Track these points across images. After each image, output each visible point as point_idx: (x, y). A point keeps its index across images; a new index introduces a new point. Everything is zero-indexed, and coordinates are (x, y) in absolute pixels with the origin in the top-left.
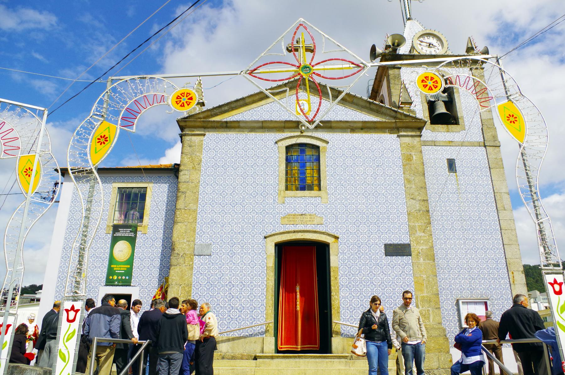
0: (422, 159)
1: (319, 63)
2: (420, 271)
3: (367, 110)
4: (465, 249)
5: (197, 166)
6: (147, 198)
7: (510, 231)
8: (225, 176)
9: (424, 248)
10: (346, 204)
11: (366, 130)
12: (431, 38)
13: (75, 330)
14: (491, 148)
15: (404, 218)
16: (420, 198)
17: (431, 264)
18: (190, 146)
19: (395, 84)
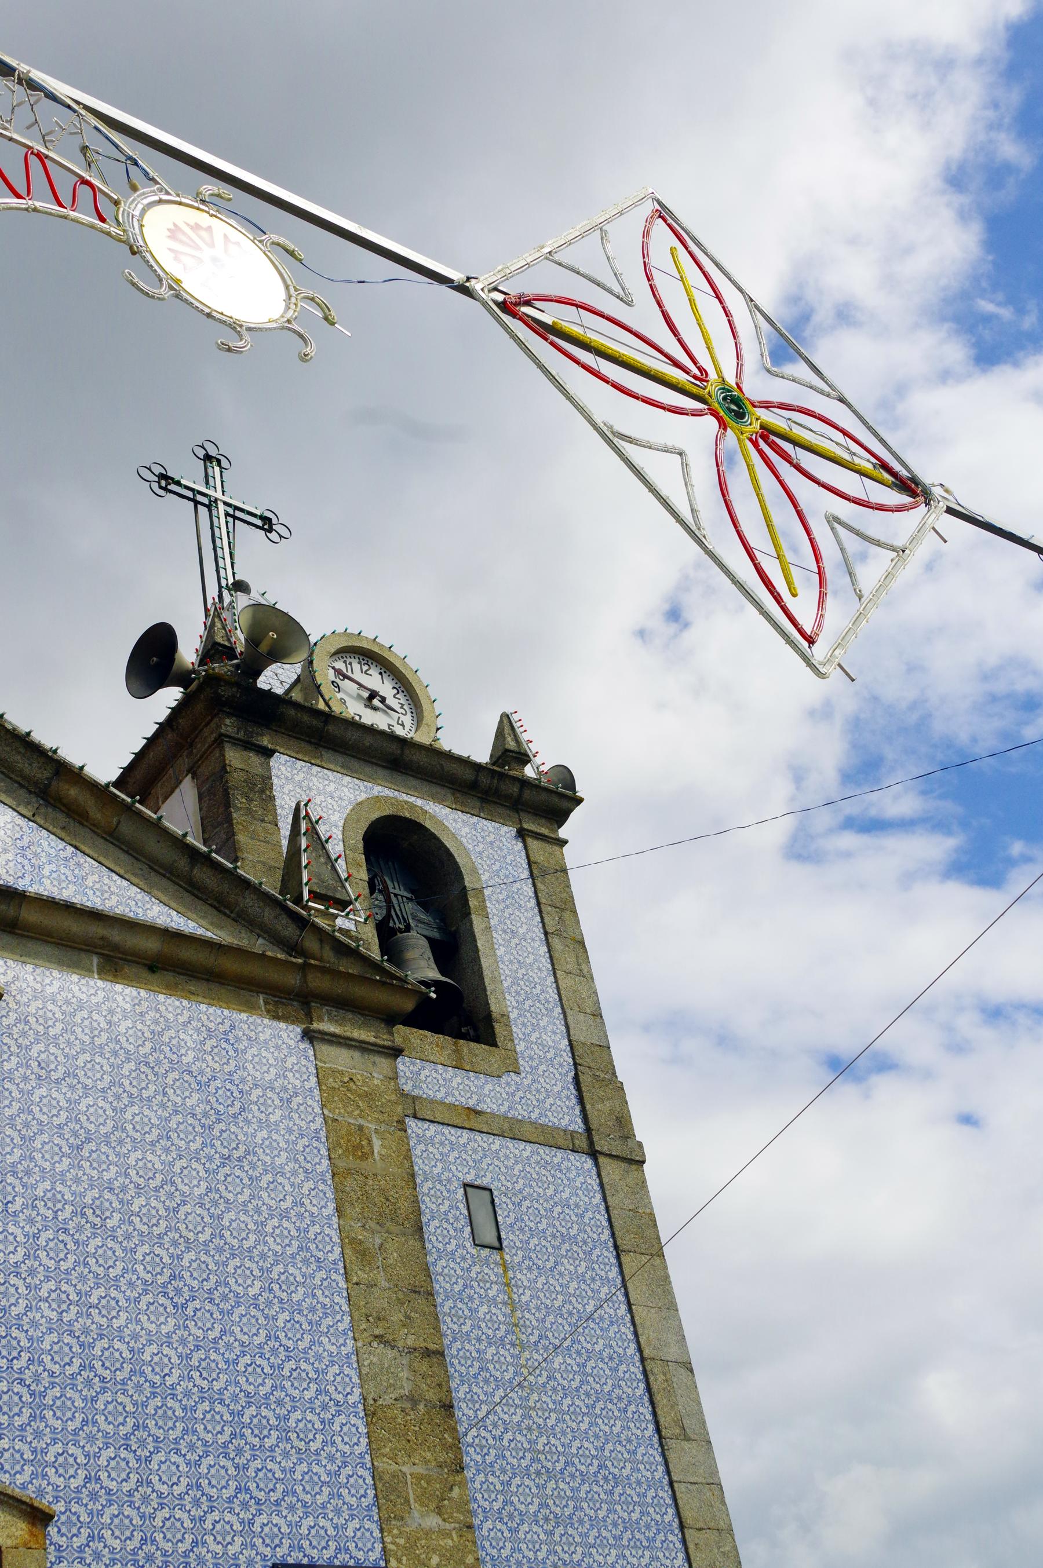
0: (408, 1157)
3: (172, 887)
7: (713, 1536)
10: (86, 1331)
11: (169, 976)
12: (374, 672)
15: (352, 1433)
16: (411, 1341)
19: (250, 812)
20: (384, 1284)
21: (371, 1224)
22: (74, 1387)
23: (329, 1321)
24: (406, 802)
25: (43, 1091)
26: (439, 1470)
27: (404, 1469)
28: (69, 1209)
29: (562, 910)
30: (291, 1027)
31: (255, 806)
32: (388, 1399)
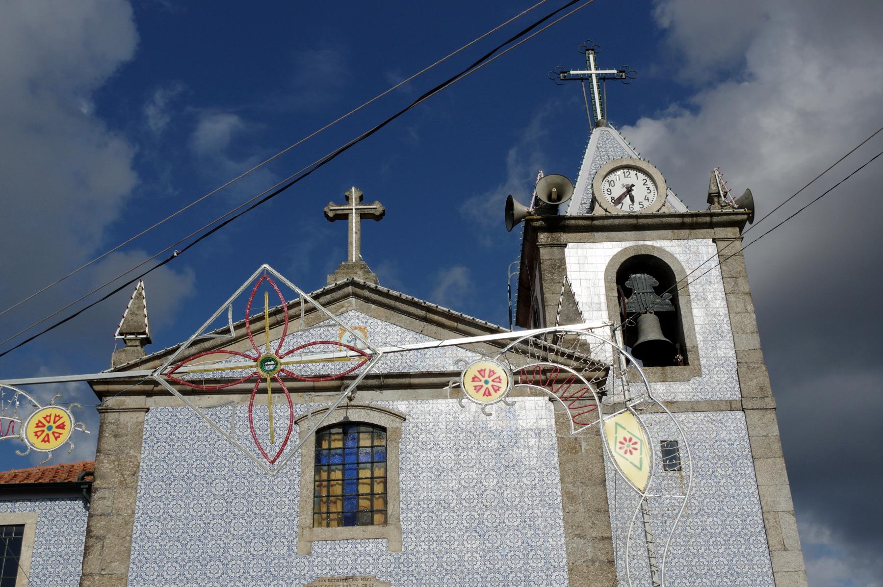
1: (292, 352)
5: (129, 480)
6: (23, 549)
8: (187, 498)
14: (756, 413)
16: (593, 535)
18: (115, 436)
19: (552, 280)
20: (582, 510)
21: (578, 484)
22: (434, 575)
23: (553, 531)
25: (424, 455)
28: (434, 502)
29: (737, 278)
31: (556, 276)
32: (580, 562)
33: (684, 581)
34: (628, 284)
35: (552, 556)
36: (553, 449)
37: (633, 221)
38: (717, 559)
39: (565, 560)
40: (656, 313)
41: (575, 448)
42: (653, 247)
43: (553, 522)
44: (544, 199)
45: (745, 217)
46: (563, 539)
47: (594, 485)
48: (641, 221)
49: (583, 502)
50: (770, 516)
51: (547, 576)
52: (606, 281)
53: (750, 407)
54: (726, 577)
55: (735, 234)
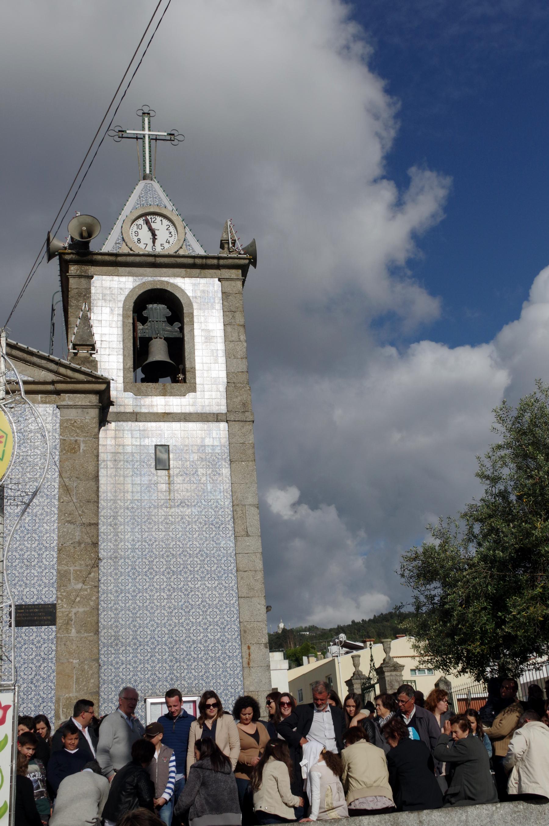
2: (70, 653)
4: (170, 608)
9: (81, 610)
13: (6, 737)
15: (51, 557)
17: (91, 639)
21: (74, 478)
23: (48, 517)
24: (159, 281)
26: (86, 567)
27: (70, 568)
30: (51, 406)
32: (68, 544)
33: (161, 560)
34: (145, 314)
35: (45, 538)
36: (55, 449)
37: (151, 259)
38: (191, 543)
39: (55, 542)
40: (166, 339)
41: (74, 448)
42: (168, 283)
43: (49, 510)
44: (77, 238)
45: (247, 261)
46: (56, 525)
47: (87, 480)
48: (159, 260)
49: (76, 494)
50: (238, 509)
51: (39, 555)
52: (192, 315)
53: (232, 419)
54: (197, 557)
55: (237, 275)
